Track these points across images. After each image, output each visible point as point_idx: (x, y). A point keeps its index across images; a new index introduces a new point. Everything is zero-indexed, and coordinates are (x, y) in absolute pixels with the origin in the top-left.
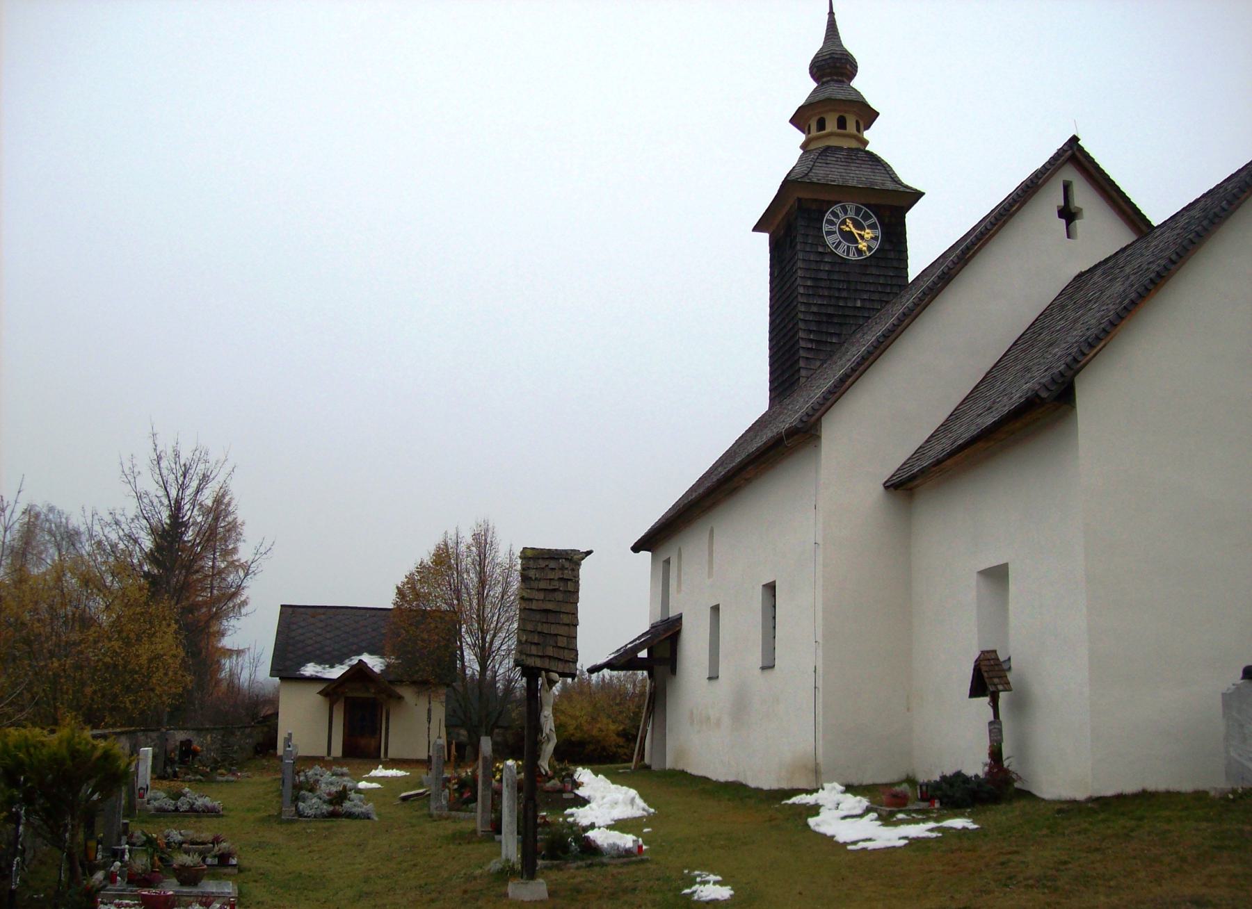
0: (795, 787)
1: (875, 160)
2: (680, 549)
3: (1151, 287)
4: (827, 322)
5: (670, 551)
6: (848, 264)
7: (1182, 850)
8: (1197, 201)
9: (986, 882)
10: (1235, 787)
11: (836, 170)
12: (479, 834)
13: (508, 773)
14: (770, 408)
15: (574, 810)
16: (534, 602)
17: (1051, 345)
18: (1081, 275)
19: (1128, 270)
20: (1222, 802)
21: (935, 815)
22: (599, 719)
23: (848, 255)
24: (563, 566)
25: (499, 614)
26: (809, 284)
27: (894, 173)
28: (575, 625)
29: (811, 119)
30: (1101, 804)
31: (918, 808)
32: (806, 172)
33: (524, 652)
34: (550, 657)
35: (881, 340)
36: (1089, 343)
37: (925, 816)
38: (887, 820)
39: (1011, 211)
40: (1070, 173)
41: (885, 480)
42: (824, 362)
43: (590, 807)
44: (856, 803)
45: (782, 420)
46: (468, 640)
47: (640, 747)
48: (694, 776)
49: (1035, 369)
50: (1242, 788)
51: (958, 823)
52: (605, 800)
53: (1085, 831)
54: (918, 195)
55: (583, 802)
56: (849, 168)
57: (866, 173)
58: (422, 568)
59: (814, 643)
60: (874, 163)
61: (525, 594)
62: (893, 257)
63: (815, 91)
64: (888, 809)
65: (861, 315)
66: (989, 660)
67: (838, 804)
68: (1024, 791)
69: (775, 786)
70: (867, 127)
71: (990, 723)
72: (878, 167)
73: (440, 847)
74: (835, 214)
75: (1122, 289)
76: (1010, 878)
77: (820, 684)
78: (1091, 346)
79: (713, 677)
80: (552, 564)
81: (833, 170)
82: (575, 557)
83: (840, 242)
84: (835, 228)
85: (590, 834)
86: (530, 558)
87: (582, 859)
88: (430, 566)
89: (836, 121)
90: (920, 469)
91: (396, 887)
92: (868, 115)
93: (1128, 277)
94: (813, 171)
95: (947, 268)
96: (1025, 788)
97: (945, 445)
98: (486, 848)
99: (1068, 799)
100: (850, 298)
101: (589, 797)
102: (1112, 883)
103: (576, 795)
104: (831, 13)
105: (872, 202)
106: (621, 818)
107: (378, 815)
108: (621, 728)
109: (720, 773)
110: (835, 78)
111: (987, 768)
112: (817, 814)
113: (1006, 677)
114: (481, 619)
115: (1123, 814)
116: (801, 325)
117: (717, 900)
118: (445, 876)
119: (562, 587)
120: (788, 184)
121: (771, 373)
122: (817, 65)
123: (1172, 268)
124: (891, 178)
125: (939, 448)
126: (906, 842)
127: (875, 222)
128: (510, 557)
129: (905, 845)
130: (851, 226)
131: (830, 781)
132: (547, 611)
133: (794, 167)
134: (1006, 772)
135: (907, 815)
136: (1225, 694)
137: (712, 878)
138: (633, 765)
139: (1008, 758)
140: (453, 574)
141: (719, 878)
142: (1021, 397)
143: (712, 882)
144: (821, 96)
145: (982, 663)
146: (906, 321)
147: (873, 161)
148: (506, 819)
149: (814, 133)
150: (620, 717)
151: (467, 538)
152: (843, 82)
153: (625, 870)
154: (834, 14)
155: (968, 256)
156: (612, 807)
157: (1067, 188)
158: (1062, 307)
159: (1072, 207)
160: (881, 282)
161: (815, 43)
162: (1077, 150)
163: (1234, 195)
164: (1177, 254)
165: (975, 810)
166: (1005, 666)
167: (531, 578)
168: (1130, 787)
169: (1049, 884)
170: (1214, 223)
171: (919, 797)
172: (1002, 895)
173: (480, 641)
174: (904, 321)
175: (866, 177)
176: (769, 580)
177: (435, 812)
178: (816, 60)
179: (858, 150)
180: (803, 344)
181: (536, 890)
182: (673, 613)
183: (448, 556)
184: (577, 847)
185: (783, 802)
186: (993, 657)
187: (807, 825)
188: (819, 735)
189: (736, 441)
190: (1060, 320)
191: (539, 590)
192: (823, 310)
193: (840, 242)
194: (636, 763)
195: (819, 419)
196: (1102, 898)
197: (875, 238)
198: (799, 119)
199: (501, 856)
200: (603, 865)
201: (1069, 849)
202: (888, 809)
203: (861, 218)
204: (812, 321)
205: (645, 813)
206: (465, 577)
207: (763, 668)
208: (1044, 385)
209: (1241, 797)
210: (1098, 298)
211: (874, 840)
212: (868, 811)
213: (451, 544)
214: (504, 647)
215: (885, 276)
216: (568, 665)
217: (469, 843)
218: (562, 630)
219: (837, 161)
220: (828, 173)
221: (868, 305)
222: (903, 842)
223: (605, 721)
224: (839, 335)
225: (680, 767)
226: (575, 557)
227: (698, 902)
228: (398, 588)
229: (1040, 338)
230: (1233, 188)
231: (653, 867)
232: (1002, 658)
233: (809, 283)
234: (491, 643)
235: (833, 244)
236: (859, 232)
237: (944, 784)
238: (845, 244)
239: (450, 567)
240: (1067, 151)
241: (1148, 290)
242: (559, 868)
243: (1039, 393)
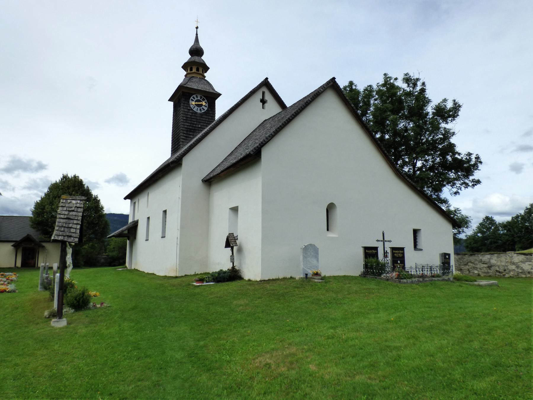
2: (139, 199)
5: (136, 200)
14: (171, 156)
23: (197, 111)
40: (264, 89)
63: (190, 58)
70: (206, 72)
71: (231, 256)
74: (194, 98)
83: (195, 107)
104: (197, 34)
120: (180, 87)
149: (189, 71)
157: (263, 93)
159: (264, 100)
161: (191, 43)
180: (182, 137)
182: (136, 219)
192: (188, 127)
198: (185, 67)
207: (162, 237)
215: (209, 119)
224: (193, 135)
233: (185, 118)
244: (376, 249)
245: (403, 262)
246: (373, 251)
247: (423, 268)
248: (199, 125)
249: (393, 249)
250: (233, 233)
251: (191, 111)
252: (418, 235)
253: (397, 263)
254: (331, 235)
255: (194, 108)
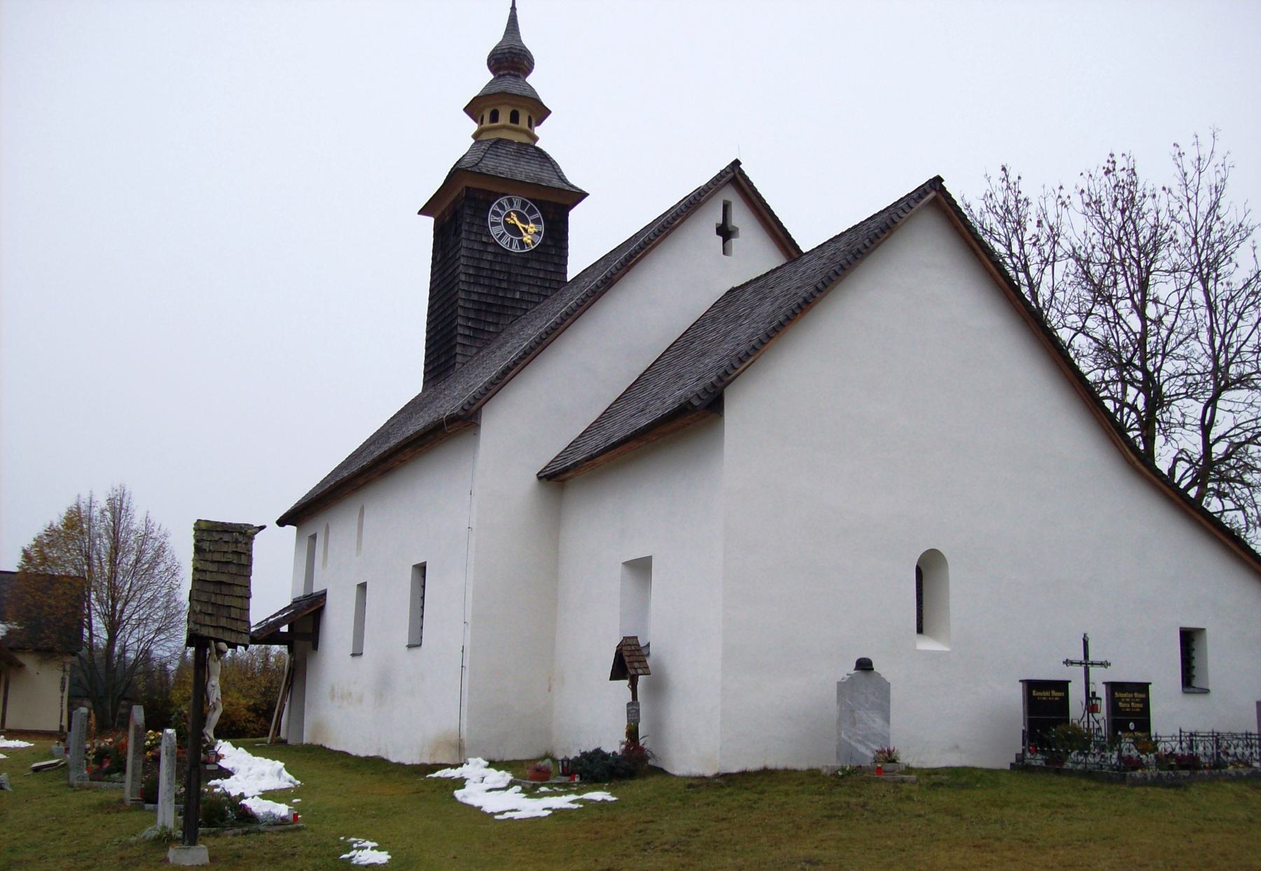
0: (438, 762)
1: (543, 156)
3: (797, 311)
4: (486, 311)
5: (316, 526)
6: (511, 256)
7: (797, 819)
8: (842, 234)
9: (626, 847)
10: (844, 765)
11: (506, 163)
12: (128, 803)
13: (168, 741)
15: (218, 781)
16: (208, 573)
17: (703, 355)
18: (733, 290)
19: (777, 291)
20: (833, 778)
21: (575, 789)
22: (230, 693)
23: (511, 247)
24: (237, 539)
25: (132, 582)
26: (471, 273)
27: (561, 172)
28: (248, 597)
29: (484, 110)
30: (727, 780)
31: (559, 782)
32: (476, 162)
33: (198, 622)
34: (223, 628)
35: (544, 336)
36: (740, 359)
37: (567, 789)
38: (531, 792)
39: (673, 225)
40: (730, 194)
41: (539, 470)
42: (480, 349)
43: (236, 778)
44: (504, 777)
45: (439, 405)
46: (98, 607)
47: (276, 722)
48: (332, 750)
49: (687, 376)
50: (850, 766)
51: (598, 796)
52: (252, 771)
53: (713, 803)
54: (582, 195)
55: (227, 774)
56: (519, 162)
57: (534, 169)
58: (52, 532)
59: (463, 624)
60: (542, 160)
61: (198, 565)
62: (553, 253)
64: (532, 782)
65: (519, 306)
66: (630, 645)
67: (483, 778)
68: (655, 767)
69: (416, 760)
70: (539, 123)
71: (629, 705)
72: (547, 164)
73: (88, 816)
74: (501, 206)
75: (771, 310)
76: (648, 843)
77: (466, 663)
78: (741, 361)
79: (357, 654)
80: (226, 537)
81: (503, 162)
82: (249, 531)
83: (504, 234)
84: (500, 220)
85: (244, 802)
86: (204, 530)
87: (240, 827)
88: (60, 530)
89: (509, 115)
90: (574, 463)
91: (48, 855)
92: (540, 112)
93: (776, 298)
94: (484, 162)
95: (610, 274)
96: (659, 765)
97: (598, 442)
98: (136, 816)
99: (697, 775)
100: (510, 290)
101: (232, 768)
102: (737, 848)
103: (220, 767)
104: (513, 8)
105: (538, 198)
106: (268, 789)
107: (11, 786)
108: (251, 703)
109: (360, 747)
110: (512, 72)
111: (623, 747)
112: (463, 787)
113: (646, 661)
114: (113, 588)
115: (747, 789)
116: (460, 312)
117: (376, 863)
118: (98, 844)
119: (235, 559)
120: (457, 173)
121: (426, 357)
122: (495, 57)
123: (818, 295)
124: (559, 176)
125: (593, 443)
126: (550, 812)
127: (539, 218)
128: (147, 525)
129: (549, 815)
130: (515, 219)
131: (475, 757)
132: (221, 583)
133: (464, 156)
134: (642, 749)
135: (550, 788)
136: (841, 682)
137: (369, 844)
138: (268, 739)
139: (643, 737)
140: (84, 539)
141: (375, 844)
142: (674, 403)
143: (370, 847)
144: (497, 89)
145: (624, 648)
146: (568, 321)
147: (542, 158)
148: (164, 786)
149: (487, 124)
150: (251, 692)
151: (102, 503)
152: (519, 77)
153: (281, 837)
154: (515, 9)
155: (631, 263)
156: (259, 779)
157: (726, 207)
158: (714, 319)
159: (729, 226)
160: (541, 276)
161: (494, 36)
162: (739, 172)
163: (876, 234)
164: (823, 283)
165: (613, 784)
166: (645, 652)
167: (205, 550)
168: (753, 765)
169: (683, 848)
170: (857, 259)
171: (561, 771)
172: (641, 858)
173: (110, 610)
174: (566, 320)
175: (534, 172)
176: (419, 561)
177: (76, 782)
178: (495, 52)
179: (528, 145)
180: (460, 330)
181: (199, 854)
182: (317, 589)
183: (80, 520)
184: (233, 815)
185: (428, 776)
186: (634, 643)
187: (454, 797)
188: (465, 709)
189: (388, 421)
190: (711, 332)
191: (213, 562)
193: (504, 234)
194: (273, 736)
195: (480, 409)
196: (730, 860)
197: (538, 233)
198: (472, 109)
199: (156, 823)
200: (259, 832)
201: (700, 819)
202: (532, 782)
203: (526, 212)
204: (470, 308)
205: (291, 785)
206: (98, 542)
207: (409, 646)
208: (697, 394)
209: (849, 773)
210: (748, 315)
211: (519, 811)
212: (511, 784)
213: (83, 507)
214: (135, 617)
216: (240, 636)
217: (118, 812)
218: (237, 602)
219: (507, 154)
220: (497, 165)
221: (526, 297)
222: (547, 813)
223: (236, 695)
224: (497, 324)
225: (319, 742)
226: (249, 531)
227: (357, 865)
228: (24, 551)
229: (692, 347)
230: (876, 228)
231: (308, 834)
232: (642, 644)
233: (471, 271)
234: (122, 611)
235: (497, 235)
236: (523, 226)
237: (584, 760)
238: (508, 236)
239: (82, 532)
240: (729, 173)
241: (794, 313)
242: (216, 835)
243: (692, 401)
244: (1063, 686)
245: (1143, 721)
246: (1053, 692)
247: (1191, 741)
248: (515, 291)
249: (1113, 687)
250: (636, 637)
251: (490, 249)
252: (1196, 645)
253: (1127, 729)
254: (926, 645)
255: (500, 239)
